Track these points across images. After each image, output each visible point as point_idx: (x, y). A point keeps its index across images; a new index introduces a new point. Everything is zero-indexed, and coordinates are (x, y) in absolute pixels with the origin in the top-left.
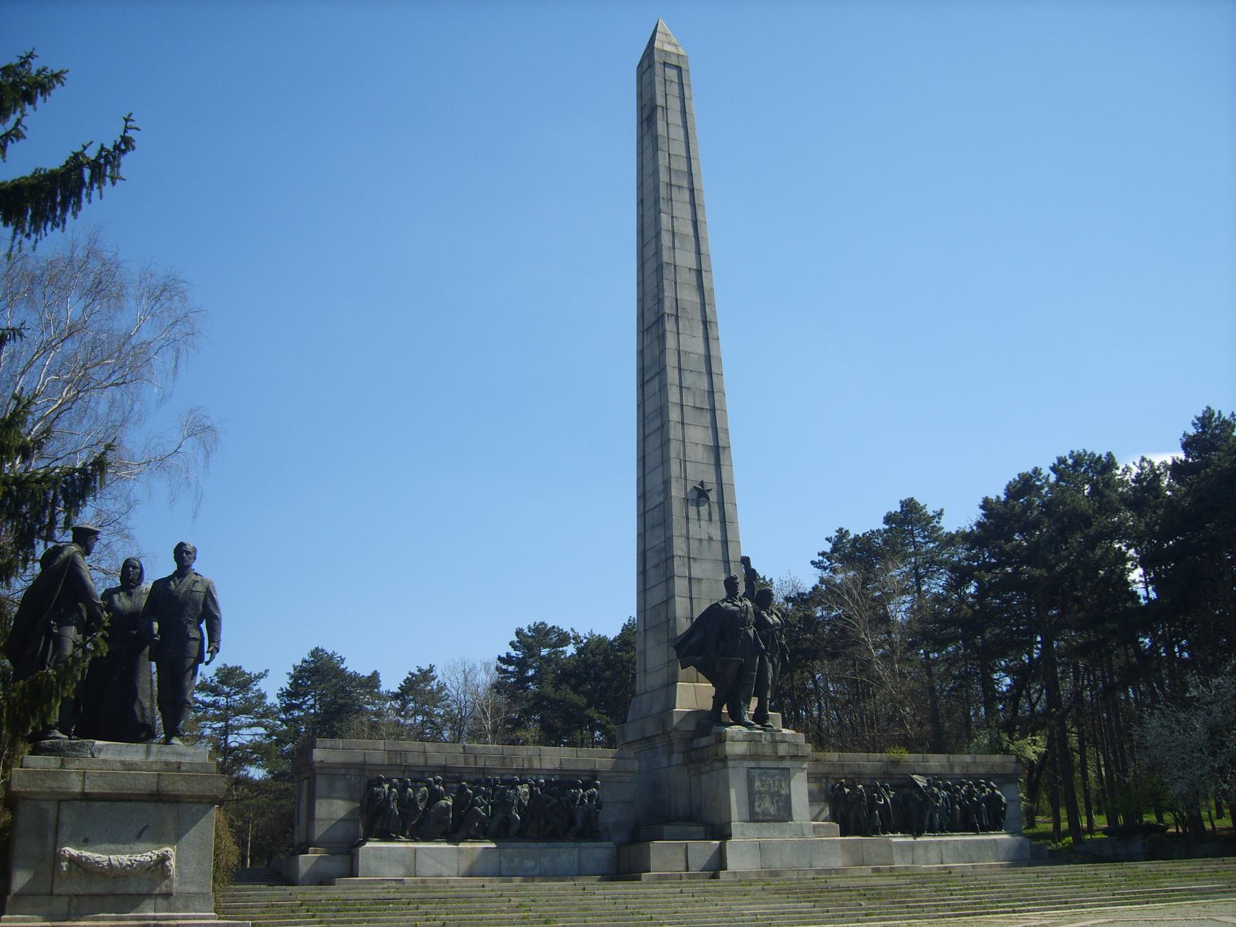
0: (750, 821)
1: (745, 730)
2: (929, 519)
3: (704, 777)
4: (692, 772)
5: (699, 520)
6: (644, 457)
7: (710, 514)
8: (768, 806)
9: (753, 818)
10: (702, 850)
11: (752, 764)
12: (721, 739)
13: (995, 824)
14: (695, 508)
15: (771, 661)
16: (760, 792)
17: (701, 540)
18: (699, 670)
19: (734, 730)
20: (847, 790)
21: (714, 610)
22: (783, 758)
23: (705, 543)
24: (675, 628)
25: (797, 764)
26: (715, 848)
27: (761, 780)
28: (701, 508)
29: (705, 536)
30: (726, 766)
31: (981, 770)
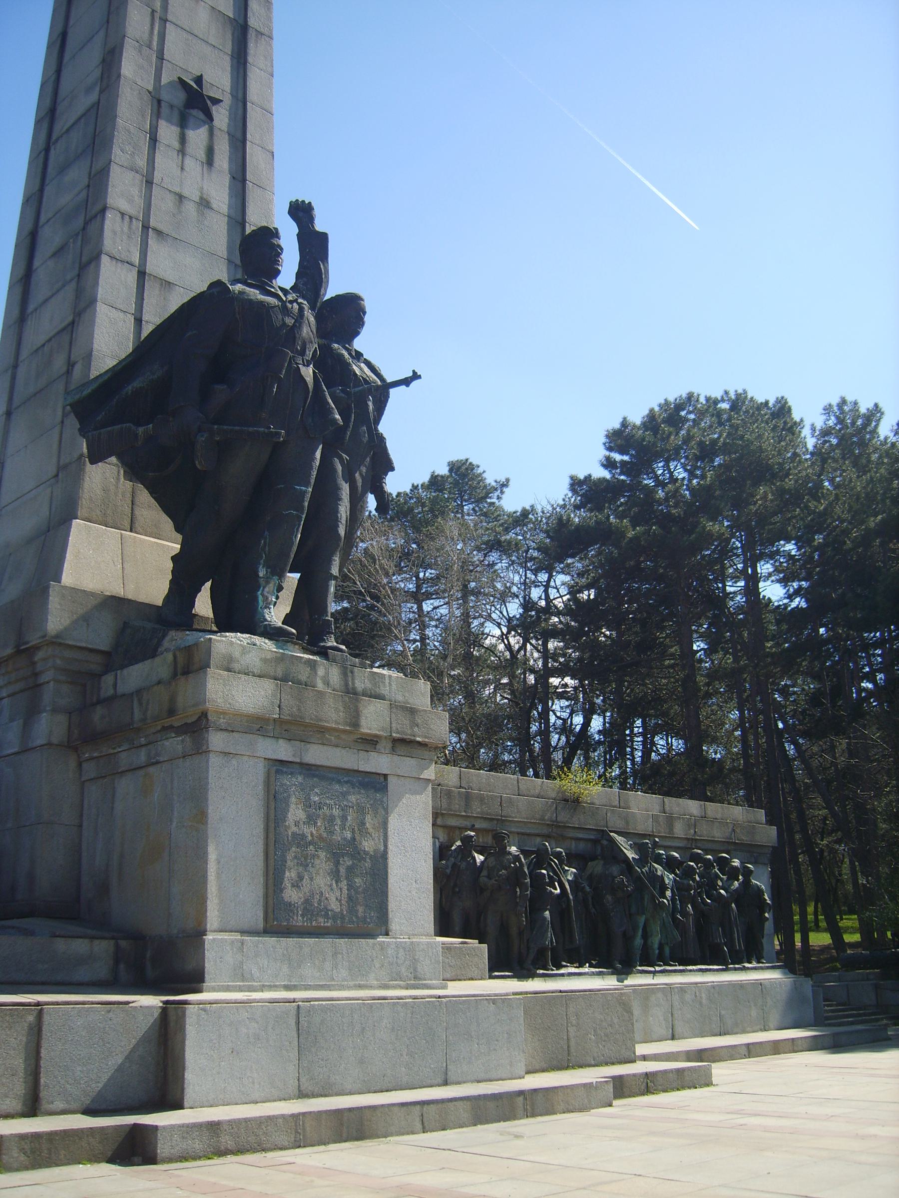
0: (268, 931)
1: (268, 645)
2: (489, 491)
3: (125, 786)
4: (90, 770)
5: (182, 152)
6: (64, 36)
7: (210, 152)
8: (320, 884)
9: (278, 921)
10: (97, 1024)
11: (283, 750)
12: (192, 665)
13: (748, 952)
14: (175, 130)
15: (350, 478)
16: (300, 840)
17: (181, 198)
18: (135, 471)
19: (232, 643)
20: (479, 858)
21: (211, 302)
22: (370, 742)
23: (190, 209)
24: (88, 357)
25: (406, 764)
26: (144, 1024)
27: (307, 804)
28: (191, 134)
29: (191, 192)
30: (200, 749)
31: (718, 834)
